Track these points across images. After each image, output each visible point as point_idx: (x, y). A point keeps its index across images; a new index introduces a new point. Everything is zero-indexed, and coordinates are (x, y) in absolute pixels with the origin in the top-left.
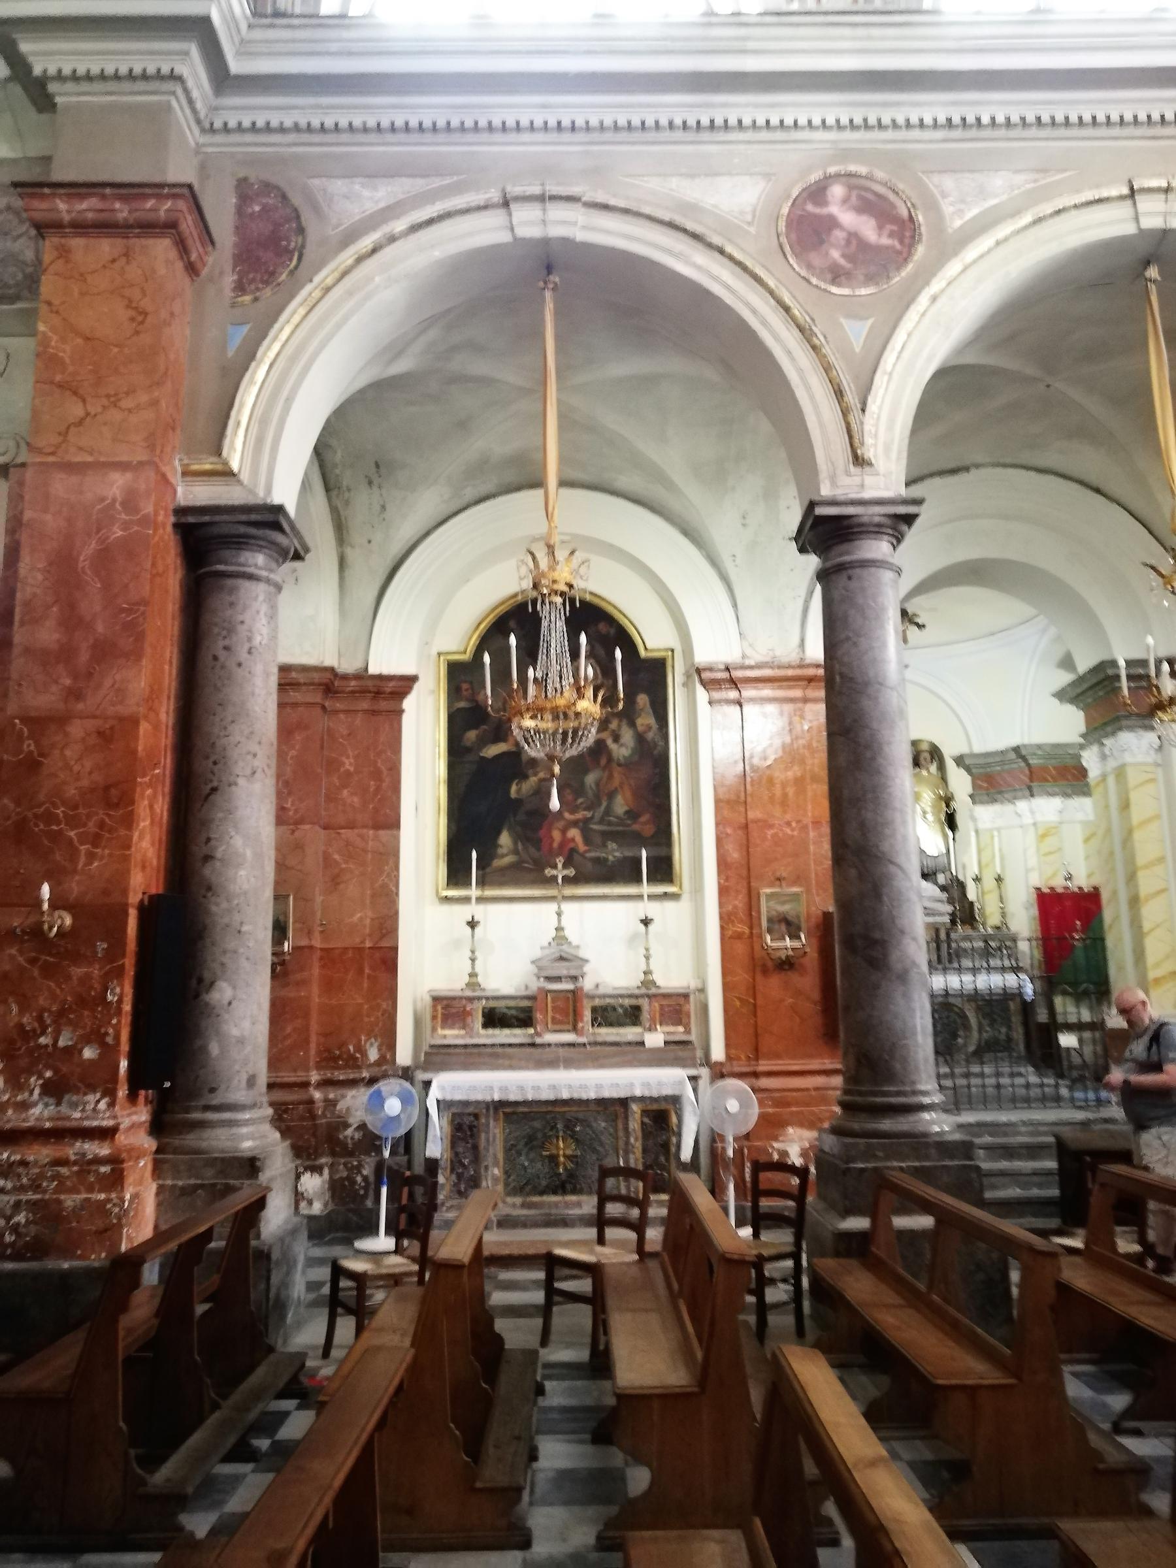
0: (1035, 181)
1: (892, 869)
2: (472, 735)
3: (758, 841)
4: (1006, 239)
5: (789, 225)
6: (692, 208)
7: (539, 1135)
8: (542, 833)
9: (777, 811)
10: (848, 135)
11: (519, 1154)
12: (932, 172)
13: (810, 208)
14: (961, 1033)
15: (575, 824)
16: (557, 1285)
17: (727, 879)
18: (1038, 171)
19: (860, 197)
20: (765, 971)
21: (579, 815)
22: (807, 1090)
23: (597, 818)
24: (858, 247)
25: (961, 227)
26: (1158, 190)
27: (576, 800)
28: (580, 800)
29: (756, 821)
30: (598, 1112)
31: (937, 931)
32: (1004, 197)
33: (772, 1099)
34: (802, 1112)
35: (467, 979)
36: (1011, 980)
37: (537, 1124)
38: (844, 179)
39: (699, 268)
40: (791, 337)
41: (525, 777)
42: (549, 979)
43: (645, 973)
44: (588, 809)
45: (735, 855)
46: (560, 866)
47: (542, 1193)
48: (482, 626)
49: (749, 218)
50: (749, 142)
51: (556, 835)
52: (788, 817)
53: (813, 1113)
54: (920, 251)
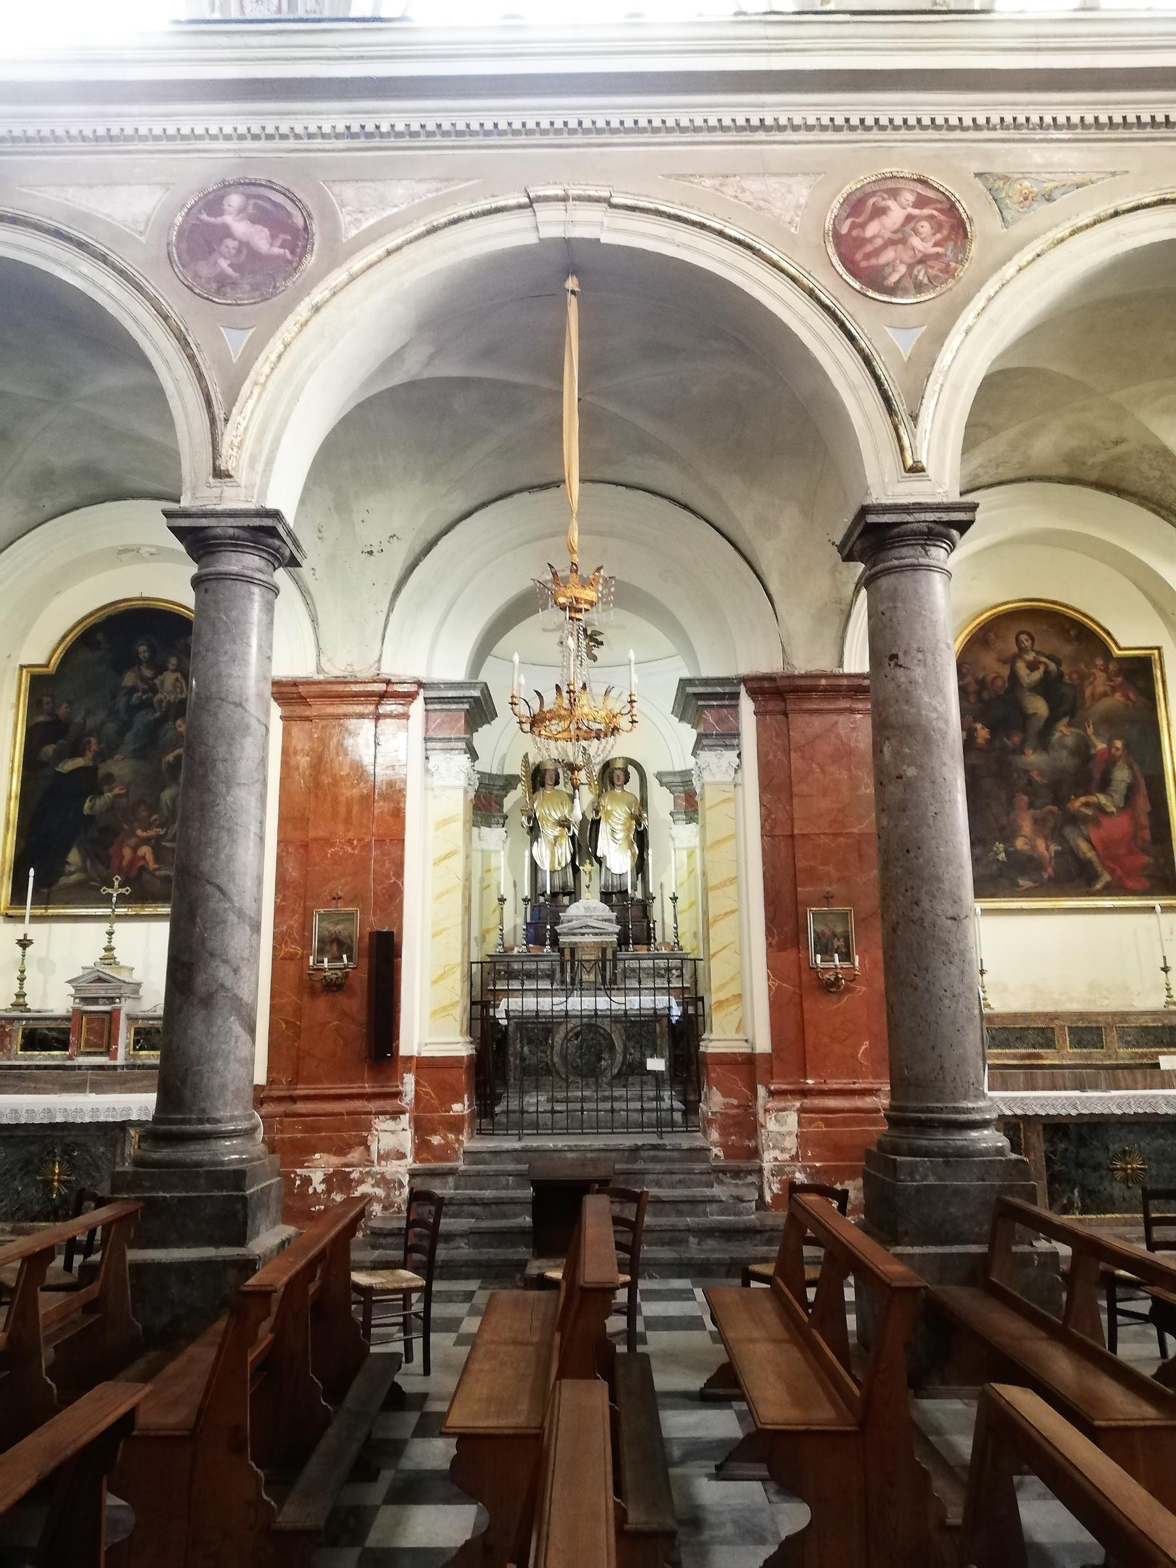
0: (438, 190)
1: (210, 889)
2: (49, 749)
3: (317, 860)
4: (399, 248)
5: (180, 235)
6: (87, 218)
7: (36, 1161)
8: (112, 851)
9: (340, 828)
10: (249, 144)
11: (14, 1178)
12: (334, 181)
13: (204, 217)
14: (605, 1055)
15: (146, 841)
16: (1120, 1305)
17: (284, 899)
18: (442, 180)
19: (256, 206)
20: (313, 993)
21: (151, 833)
22: (341, 1114)
23: (169, 837)
24: (249, 257)
25: (356, 236)
26: (557, 199)
27: (150, 816)
28: (155, 817)
29: (315, 840)
30: (98, 1137)
31: (604, 951)
32: (403, 207)
33: (302, 1123)
34: (331, 1138)
35: (14, 999)
36: (662, 1001)
37: (35, 1148)
38: (241, 188)
39: (85, 277)
40: (170, 346)
41: (102, 793)
42: (86, 1000)
43: (18, 996)
44: (161, 826)
45: (294, 874)
46: (116, 884)
47: (32, 1221)
48: (69, 638)
49: (142, 228)
50: (151, 152)
51: (127, 852)
52: (350, 835)
53: (341, 1138)
54: (310, 261)
